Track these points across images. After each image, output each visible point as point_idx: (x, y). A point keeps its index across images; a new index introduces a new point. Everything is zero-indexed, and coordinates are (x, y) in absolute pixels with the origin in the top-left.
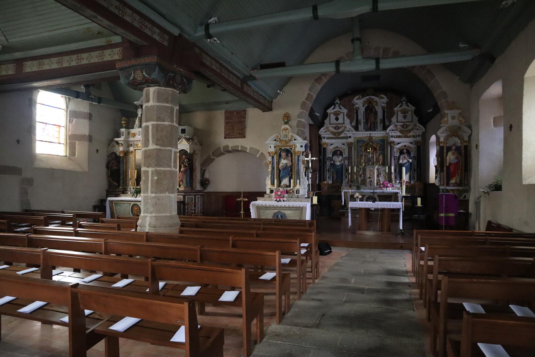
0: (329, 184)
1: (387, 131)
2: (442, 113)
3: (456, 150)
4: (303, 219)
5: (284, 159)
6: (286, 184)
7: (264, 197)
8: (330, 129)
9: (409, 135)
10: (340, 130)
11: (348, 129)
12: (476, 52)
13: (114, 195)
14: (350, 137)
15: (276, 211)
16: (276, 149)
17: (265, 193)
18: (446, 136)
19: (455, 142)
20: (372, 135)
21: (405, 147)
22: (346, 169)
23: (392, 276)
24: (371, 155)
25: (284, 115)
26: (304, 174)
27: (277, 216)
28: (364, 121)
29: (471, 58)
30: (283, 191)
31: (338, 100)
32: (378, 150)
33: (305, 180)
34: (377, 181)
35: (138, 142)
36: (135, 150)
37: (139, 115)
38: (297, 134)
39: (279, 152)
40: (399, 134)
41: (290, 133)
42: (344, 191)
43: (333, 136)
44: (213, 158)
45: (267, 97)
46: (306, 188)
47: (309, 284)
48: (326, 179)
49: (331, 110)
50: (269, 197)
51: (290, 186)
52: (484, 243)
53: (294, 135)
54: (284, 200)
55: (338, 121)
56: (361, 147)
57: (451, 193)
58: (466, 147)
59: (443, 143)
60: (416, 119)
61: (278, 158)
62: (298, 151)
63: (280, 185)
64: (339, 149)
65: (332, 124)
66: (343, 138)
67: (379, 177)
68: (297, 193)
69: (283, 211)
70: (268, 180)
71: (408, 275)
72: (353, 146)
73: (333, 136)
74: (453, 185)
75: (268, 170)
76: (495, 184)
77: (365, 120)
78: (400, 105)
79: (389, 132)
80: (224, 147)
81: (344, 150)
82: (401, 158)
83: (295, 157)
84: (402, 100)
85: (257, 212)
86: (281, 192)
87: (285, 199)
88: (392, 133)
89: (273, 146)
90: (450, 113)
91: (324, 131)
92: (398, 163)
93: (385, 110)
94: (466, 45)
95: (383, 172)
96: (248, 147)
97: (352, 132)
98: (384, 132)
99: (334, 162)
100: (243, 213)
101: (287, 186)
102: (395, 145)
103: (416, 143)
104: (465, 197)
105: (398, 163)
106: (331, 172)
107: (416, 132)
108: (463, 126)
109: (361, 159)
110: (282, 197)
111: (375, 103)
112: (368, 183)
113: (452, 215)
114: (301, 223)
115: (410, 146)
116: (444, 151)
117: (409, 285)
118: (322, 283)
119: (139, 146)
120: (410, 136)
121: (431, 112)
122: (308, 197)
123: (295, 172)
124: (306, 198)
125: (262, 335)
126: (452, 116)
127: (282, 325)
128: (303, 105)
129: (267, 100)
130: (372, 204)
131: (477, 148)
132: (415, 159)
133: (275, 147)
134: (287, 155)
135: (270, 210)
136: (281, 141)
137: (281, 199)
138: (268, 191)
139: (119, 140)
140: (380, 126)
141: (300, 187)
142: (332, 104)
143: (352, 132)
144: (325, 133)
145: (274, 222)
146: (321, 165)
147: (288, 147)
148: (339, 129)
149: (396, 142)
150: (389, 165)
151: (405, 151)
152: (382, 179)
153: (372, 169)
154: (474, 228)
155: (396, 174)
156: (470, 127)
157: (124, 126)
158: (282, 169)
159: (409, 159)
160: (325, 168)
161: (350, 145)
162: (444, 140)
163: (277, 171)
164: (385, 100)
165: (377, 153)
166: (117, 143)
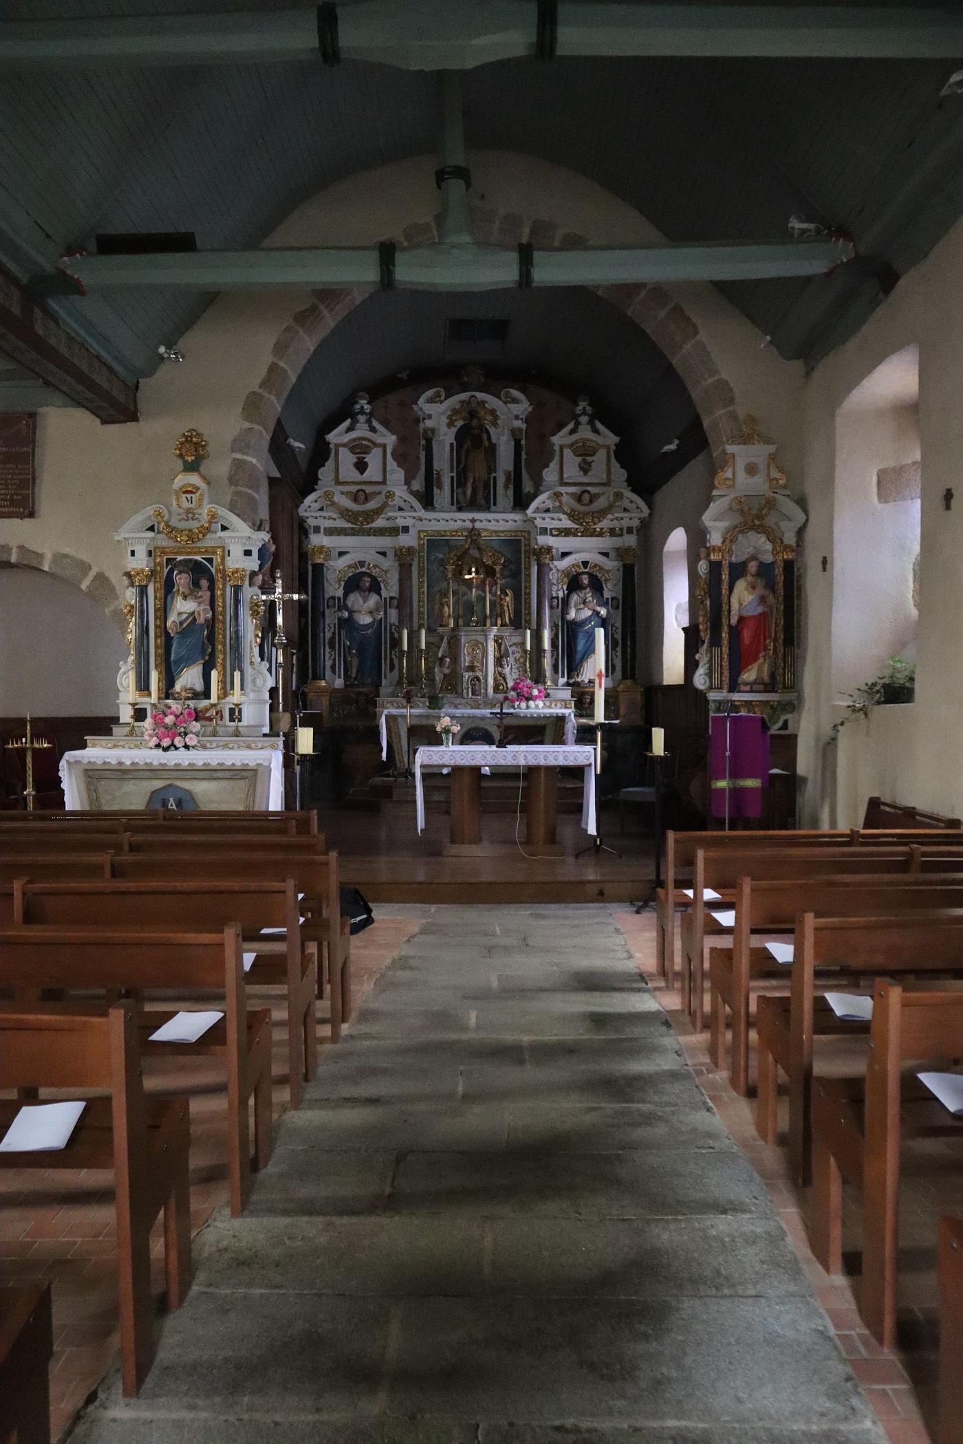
0: (334, 689)
1: (530, 511)
2: (715, 454)
3: (758, 574)
4: (258, 807)
5: (185, 598)
6: (191, 689)
7: (111, 735)
8: (336, 499)
9: (598, 527)
10: (372, 505)
11: (397, 502)
12: (843, 251)
14: (406, 529)
15: (158, 784)
16: (155, 560)
17: (115, 720)
18: (728, 530)
19: (755, 548)
20: (478, 525)
22: (392, 637)
23: (597, 994)
24: (474, 590)
25: (183, 439)
26: (256, 650)
27: (165, 803)
28: (452, 477)
29: (825, 270)
30: (182, 714)
32: (498, 575)
33: (262, 674)
34: (495, 679)
38: (232, 509)
39: (166, 571)
40: (566, 523)
41: (205, 502)
42: (386, 712)
43: (349, 525)
46: (262, 702)
47: (322, 1040)
48: (324, 674)
49: (340, 435)
50: (132, 733)
51: (206, 694)
52: (904, 867)
53: (220, 513)
54: (188, 743)
55: (365, 474)
56: (442, 563)
57: (743, 713)
58: (789, 566)
59: (720, 551)
60: (620, 474)
61: (161, 594)
62: (237, 571)
63: (170, 692)
64: (369, 568)
65: (342, 483)
66: (381, 532)
67: (502, 666)
68: (232, 720)
69: (186, 785)
70: (125, 673)
71: (650, 985)
72: (416, 559)
73: (349, 525)
74: (751, 688)
75: (124, 637)
76: (887, 681)
77: (454, 474)
78: (571, 426)
79: (534, 515)
81: (386, 572)
82: (573, 603)
83: (224, 589)
84: (579, 409)
85: (89, 789)
86: (177, 717)
87: (191, 739)
88: (544, 519)
90: (741, 454)
91: (316, 506)
92: (563, 618)
93: (523, 442)
94: (811, 226)
95: (514, 648)
96: (45, 551)
97: (414, 514)
98: (517, 516)
99: (351, 612)
100: (34, 793)
101: (196, 696)
102: (552, 559)
103: (621, 553)
104: (785, 726)
105: (563, 618)
106: (340, 648)
107: (622, 519)
108: (783, 497)
109: (442, 605)
110: (180, 735)
111: (490, 418)
112: (465, 685)
113: (751, 783)
114: (256, 821)
115: (603, 566)
116: (723, 577)
117: (665, 1020)
118: (367, 1036)
120: (601, 529)
121: (672, 452)
122: (273, 733)
123: (224, 646)
124: (265, 735)
125: (187, 1267)
127: (253, 1213)
128: (252, 406)
130: (496, 751)
131: (824, 569)
132: (617, 608)
133: (150, 553)
134: (196, 584)
135: (138, 782)
136: (171, 531)
137: (178, 741)
138: (126, 715)
140: (504, 496)
141: (243, 699)
142: (343, 413)
143: (414, 514)
144: (321, 513)
145: (164, 823)
146: (306, 623)
147: (200, 553)
148: (366, 500)
149: (557, 549)
150: (534, 626)
151: (585, 580)
152: (511, 674)
153: (481, 639)
154: (815, 823)
155: (555, 656)
156: (802, 503)
158: (177, 633)
159: (599, 606)
160: (322, 635)
161: (404, 558)
162: (724, 541)
163: (159, 641)
164: (523, 407)
165: (496, 584)
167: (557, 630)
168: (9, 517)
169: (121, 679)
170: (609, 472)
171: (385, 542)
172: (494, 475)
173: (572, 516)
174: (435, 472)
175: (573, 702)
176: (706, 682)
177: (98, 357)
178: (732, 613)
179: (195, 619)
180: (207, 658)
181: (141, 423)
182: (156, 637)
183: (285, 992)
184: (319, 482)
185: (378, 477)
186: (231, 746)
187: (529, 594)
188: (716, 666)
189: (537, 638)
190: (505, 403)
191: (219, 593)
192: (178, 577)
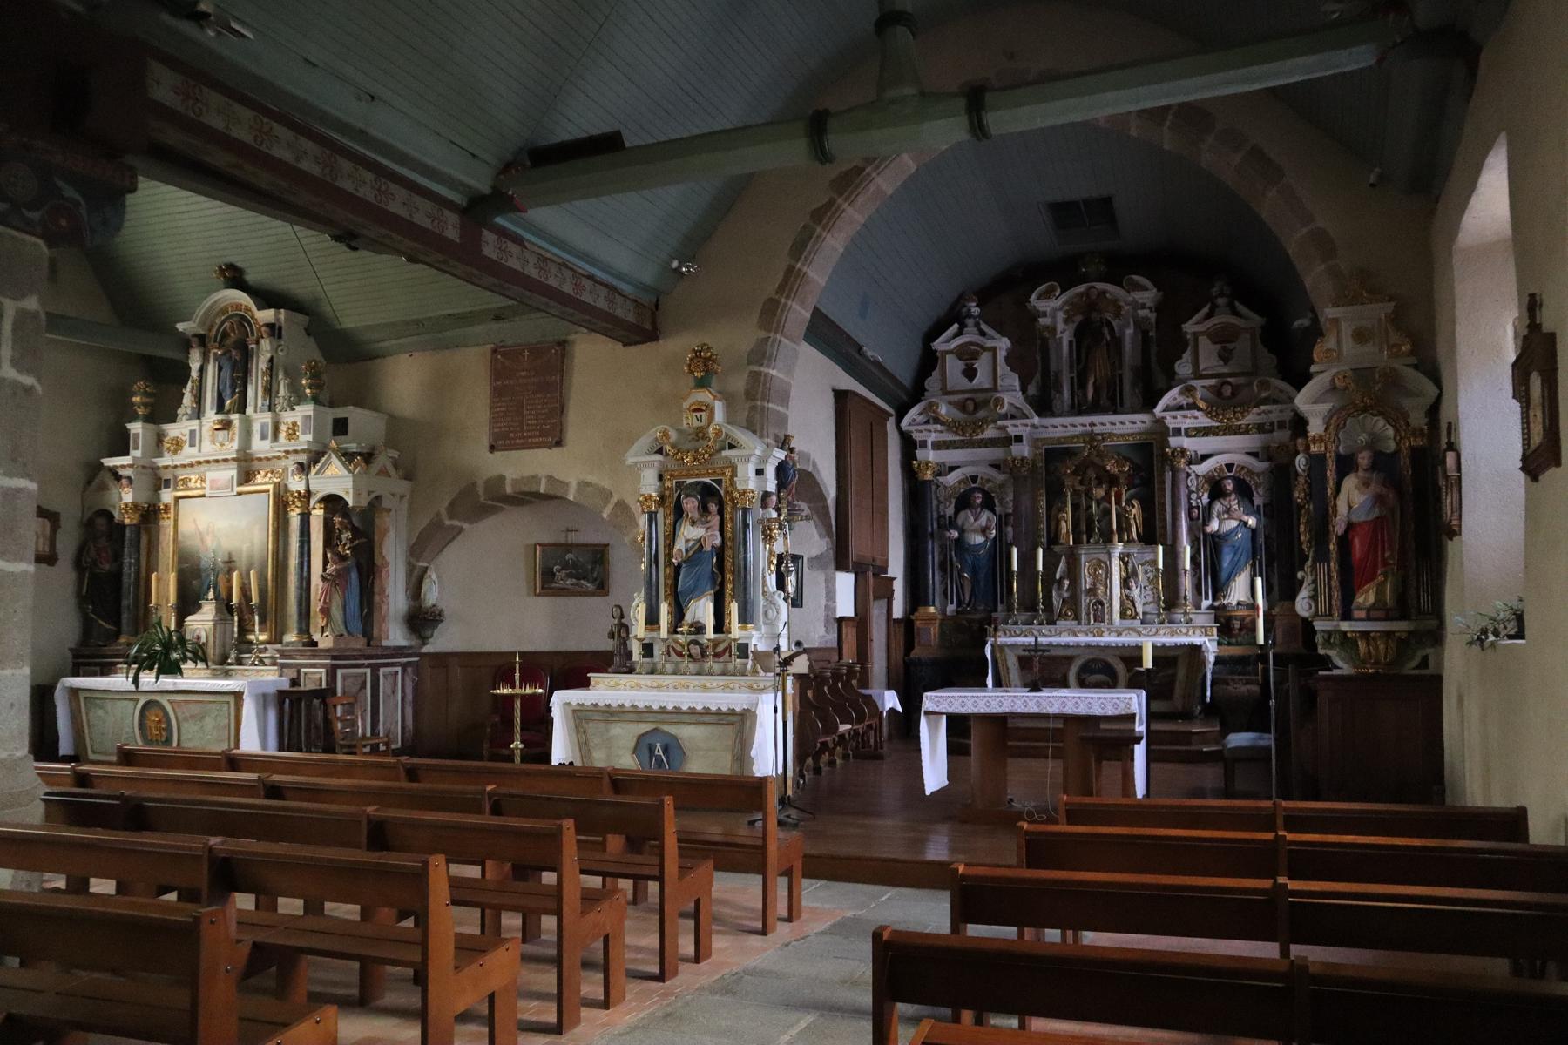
1: (1158, 410)
3: (1374, 467)
5: (693, 523)
13: (98, 669)
15: (645, 728)
18: (1331, 413)
21: (1230, 471)
28: (1072, 378)
31: (974, 304)
35: (188, 470)
36: (177, 499)
37: (194, 374)
39: (676, 495)
40: (1203, 421)
44: (453, 527)
45: (623, 286)
55: (974, 382)
60: (1268, 359)
61: (670, 520)
67: (1129, 588)
69: (672, 729)
74: (1368, 614)
77: (1074, 375)
78: (1206, 310)
80: (488, 482)
82: (1215, 514)
84: (1215, 291)
85: (578, 733)
91: (921, 418)
98: (1145, 417)
104: (1424, 663)
107: (1270, 412)
119: (191, 485)
126: (1354, 331)
129: (620, 294)
133: (661, 478)
134: (704, 509)
135: (624, 725)
139: (118, 464)
142: (953, 316)
151: (1229, 485)
153: (1104, 557)
157: (140, 411)
159: (1247, 514)
166: (115, 474)
167: (1199, 544)
168: (538, 447)
173: (1210, 413)
174: (1052, 373)
175: (1215, 629)
176: (1311, 608)
177: (591, 277)
180: (717, 588)
181: (661, 342)
183: (521, 1004)
184: (926, 393)
186: (731, 686)
189: (1172, 555)
190: (1129, 292)
191: (728, 516)
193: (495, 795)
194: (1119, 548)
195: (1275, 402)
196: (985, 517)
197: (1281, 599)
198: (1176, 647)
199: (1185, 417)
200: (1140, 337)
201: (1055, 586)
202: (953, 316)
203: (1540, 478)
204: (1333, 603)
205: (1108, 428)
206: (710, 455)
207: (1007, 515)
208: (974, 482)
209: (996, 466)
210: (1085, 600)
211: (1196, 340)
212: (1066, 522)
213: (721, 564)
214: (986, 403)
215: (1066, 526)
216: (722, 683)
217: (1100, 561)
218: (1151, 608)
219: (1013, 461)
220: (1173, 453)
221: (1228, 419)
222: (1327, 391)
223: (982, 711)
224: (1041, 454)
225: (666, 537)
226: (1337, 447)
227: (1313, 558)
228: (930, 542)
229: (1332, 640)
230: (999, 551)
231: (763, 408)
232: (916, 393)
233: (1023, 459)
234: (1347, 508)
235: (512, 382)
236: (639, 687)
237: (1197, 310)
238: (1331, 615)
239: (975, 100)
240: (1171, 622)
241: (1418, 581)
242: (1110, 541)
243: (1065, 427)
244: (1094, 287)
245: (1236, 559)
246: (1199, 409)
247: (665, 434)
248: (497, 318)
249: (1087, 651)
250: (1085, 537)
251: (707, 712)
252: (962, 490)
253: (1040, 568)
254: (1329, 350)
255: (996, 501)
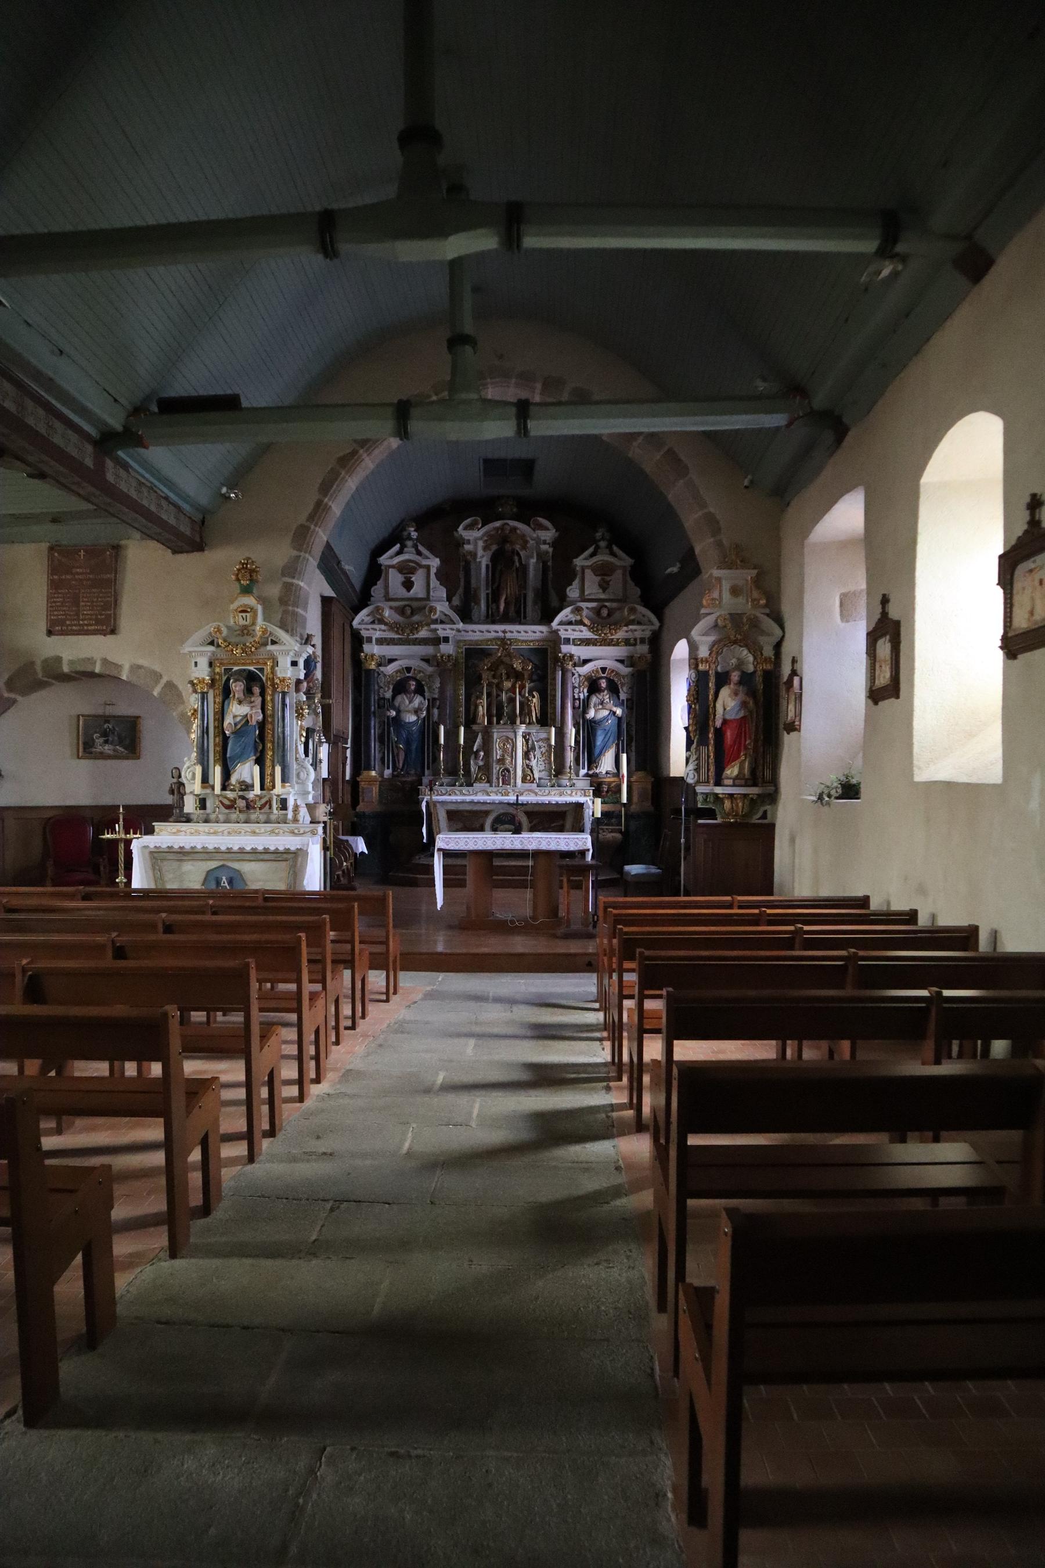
3: (740, 683)
5: (240, 702)
15: (213, 865)
19: (738, 659)
27: (218, 882)
28: (487, 594)
31: (413, 529)
34: (523, 771)
39: (224, 678)
44: (8, 699)
45: (186, 507)
61: (219, 700)
63: (226, 784)
67: (529, 759)
69: (236, 865)
74: (734, 782)
75: (189, 737)
77: (489, 591)
78: (591, 550)
82: (592, 705)
84: (598, 535)
85: (154, 869)
89: (203, 662)
91: (369, 619)
95: (540, 743)
98: (544, 628)
104: (764, 816)
107: (636, 630)
123: (273, 742)
133: (211, 664)
134: (249, 691)
142: (394, 538)
151: (603, 684)
152: (538, 765)
153: (511, 735)
163: (217, 739)
164: (549, 534)
169: (186, 773)
170: (625, 589)
171: (428, 650)
172: (525, 592)
173: (592, 628)
174: (472, 589)
175: (591, 791)
176: (694, 776)
177: (166, 498)
178: (717, 717)
179: (247, 721)
180: (258, 755)
181: (206, 552)
182: (215, 737)
183: (283, 1046)
184: (372, 599)
185: (422, 595)
187: (555, 696)
188: (703, 763)
189: (561, 735)
190: (534, 530)
191: (269, 698)
192: (233, 685)
193: (214, 906)
194: (522, 729)
195: (639, 623)
196: (418, 700)
197: (637, 770)
198: (566, 804)
199: (574, 630)
200: (541, 564)
201: (473, 757)
202: (394, 538)
203: (880, 703)
204: (710, 774)
205: (515, 635)
206: (256, 649)
207: (434, 699)
208: (409, 672)
209: (426, 660)
210: (496, 768)
211: (583, 573)
212: (483, 707)
213: (262, 737)
214: (421, 609)
215: (482, 710)
216: (269, 829)
217: (508, 738)
218: (544, 774)
219: (442, 657)
220: (564, 657)
221: (605, 634)
222: (709, 629)
223: (480, 848)
224: (462, 652)
225: (215, 714)
226: (716, 667)
227: (697, 742)
228: (373, 719)
229: (708, 800)
230: (428, 729)
231: (294, 611)
232: (364, 600)
233: (449, 656)
234: (723, 709)
235: (68, 577)
236: (198, 833)
237: (583, 551)
238: (708, 782)
239: (523, 410)
240: (559, 786)
241: (764, 761)
242: (513, 723)
243: (482, 632)
244: (508, 524)
245: (606, 739)
246: (585, 625)
247: (219, 630)
248: (55, 520)
249: (500, 806)
250: (495, 719)
251: (266, 851)
252: (398, 678)
253: (462, 742)
254: (713, 599)
255: (426, 688)
